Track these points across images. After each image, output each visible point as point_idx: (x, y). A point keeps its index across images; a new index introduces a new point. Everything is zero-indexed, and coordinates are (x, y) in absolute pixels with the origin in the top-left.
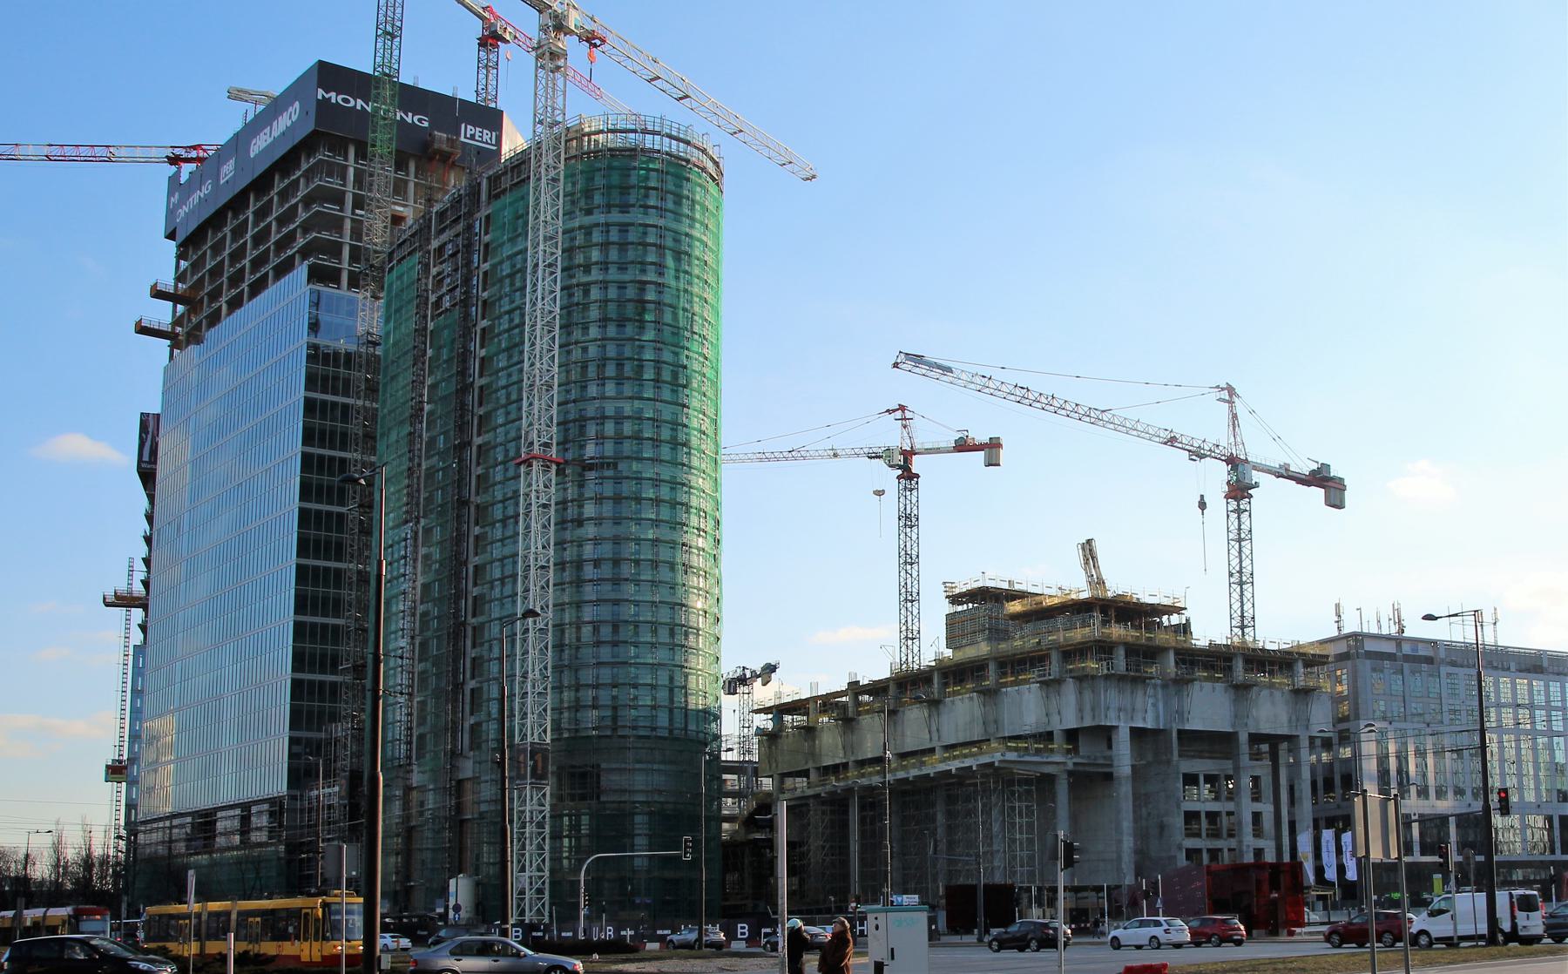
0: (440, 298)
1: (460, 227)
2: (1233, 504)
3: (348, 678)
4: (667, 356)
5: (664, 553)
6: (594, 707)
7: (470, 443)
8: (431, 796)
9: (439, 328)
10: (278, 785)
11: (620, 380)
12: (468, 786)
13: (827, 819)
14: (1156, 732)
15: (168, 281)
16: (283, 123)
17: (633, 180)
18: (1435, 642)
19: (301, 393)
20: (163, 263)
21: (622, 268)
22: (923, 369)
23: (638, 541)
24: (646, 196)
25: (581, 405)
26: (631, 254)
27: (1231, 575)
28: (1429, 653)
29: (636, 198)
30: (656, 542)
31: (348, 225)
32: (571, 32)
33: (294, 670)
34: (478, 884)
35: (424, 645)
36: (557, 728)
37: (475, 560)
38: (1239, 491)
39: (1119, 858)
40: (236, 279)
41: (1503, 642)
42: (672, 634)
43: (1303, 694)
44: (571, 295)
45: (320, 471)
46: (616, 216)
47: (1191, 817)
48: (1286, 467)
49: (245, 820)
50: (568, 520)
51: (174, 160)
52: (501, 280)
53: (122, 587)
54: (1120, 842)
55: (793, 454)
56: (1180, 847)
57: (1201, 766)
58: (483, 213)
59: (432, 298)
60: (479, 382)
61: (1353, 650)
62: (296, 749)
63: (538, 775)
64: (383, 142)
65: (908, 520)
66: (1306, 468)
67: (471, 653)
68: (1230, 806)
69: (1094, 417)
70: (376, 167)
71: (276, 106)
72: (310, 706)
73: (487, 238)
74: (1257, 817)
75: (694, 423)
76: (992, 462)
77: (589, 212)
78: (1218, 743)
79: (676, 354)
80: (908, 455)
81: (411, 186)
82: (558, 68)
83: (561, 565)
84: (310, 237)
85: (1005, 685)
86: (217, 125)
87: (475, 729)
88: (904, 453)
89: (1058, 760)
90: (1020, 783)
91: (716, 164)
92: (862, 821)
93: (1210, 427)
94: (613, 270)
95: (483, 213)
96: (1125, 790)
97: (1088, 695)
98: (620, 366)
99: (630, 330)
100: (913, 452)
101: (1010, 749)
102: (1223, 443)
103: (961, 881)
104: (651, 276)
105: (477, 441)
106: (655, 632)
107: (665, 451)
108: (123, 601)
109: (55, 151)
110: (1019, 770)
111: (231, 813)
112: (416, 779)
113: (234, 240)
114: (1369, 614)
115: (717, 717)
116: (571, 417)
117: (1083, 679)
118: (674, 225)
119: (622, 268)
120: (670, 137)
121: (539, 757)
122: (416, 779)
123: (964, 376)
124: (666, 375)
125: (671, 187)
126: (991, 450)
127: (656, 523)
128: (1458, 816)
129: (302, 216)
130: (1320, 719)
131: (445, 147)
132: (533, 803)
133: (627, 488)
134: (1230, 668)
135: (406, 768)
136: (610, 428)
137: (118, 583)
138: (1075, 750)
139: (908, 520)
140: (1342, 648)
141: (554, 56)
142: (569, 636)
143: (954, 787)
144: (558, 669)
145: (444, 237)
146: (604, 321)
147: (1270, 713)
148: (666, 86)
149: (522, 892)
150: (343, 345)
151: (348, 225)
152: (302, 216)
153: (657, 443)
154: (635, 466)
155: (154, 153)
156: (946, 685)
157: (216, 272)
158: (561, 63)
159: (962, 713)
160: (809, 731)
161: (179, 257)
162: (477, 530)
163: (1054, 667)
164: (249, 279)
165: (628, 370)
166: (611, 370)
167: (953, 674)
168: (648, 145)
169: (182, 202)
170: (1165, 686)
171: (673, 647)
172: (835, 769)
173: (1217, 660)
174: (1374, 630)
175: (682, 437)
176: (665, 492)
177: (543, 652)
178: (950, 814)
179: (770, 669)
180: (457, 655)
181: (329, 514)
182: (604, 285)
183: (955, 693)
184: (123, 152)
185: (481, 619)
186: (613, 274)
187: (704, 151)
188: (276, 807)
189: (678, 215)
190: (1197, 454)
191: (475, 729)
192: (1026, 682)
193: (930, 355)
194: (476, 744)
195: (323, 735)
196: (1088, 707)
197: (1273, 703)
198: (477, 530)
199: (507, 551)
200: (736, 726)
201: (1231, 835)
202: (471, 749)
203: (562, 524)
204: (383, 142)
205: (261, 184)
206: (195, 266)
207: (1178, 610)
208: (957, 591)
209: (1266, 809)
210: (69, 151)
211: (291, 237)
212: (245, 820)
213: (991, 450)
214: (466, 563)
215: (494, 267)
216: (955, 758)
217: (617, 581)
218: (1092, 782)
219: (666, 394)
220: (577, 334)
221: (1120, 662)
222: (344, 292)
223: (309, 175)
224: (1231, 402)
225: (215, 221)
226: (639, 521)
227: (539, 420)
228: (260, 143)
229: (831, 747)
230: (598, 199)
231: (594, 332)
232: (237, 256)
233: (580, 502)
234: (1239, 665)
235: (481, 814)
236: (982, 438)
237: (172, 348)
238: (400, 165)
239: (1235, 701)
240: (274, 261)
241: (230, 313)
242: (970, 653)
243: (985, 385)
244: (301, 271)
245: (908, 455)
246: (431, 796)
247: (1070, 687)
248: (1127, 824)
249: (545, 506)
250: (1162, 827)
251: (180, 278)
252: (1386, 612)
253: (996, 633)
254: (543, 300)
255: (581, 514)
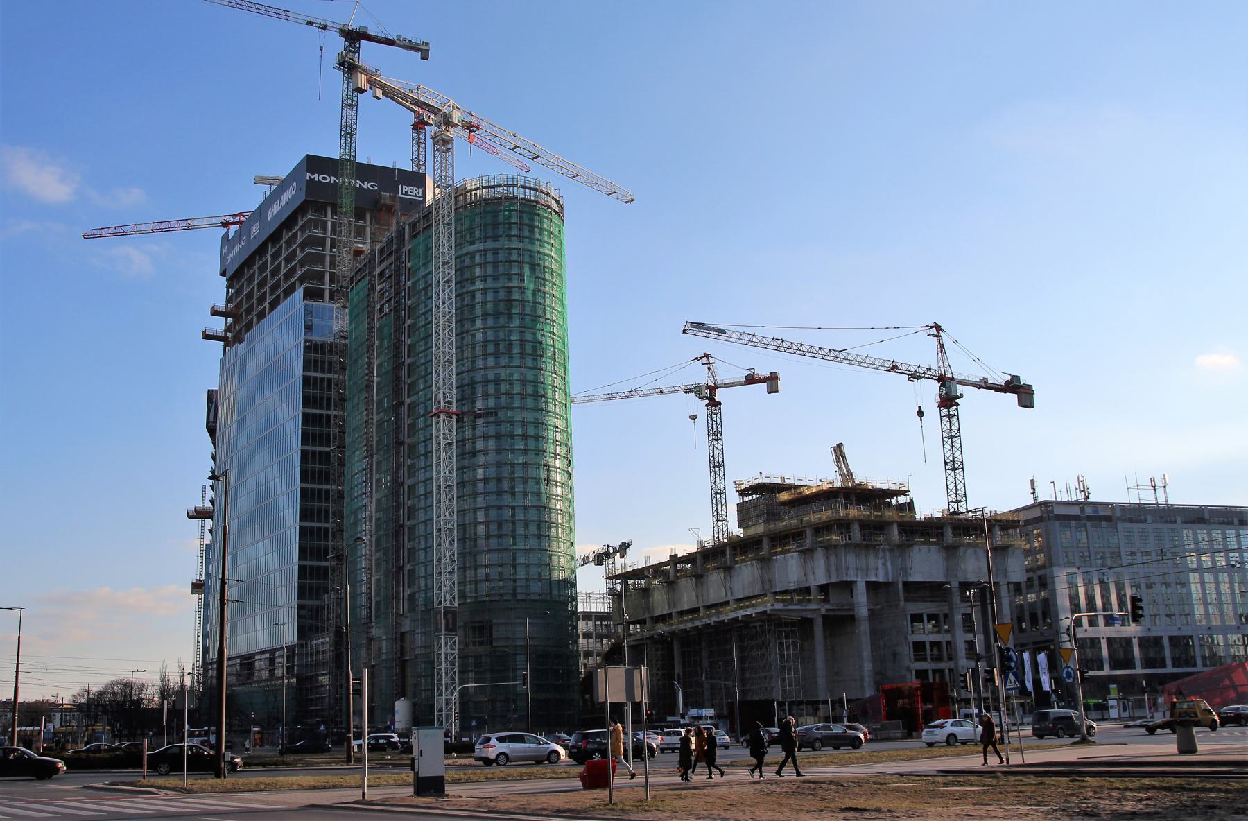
0: (382, 306)
1: (393, 258)
2: (945, 412)
3: (334, 563)
4: (529, 337)
5: (532, 472)
6: (487, 580)
7: (403, 403)
8: (384, 644)
9: (390, 321)
10: (292, 638)
11: (497, 355)
12: (408, 636)
13: (659, 653)
14: (886, 585)
15: (221, 303)
16: (287, 196)
17: (501, 219)
18: (1111, 504)
19: (300, 373)
20: (218, 292)
21: (496, 279)
22: (705, 333)
23: (513, 465)
24: (510, 229)
25: (472, 374)
26: (501, 269)
27: (946, 463)
28: (1109, 513)
29: (508, 227)
30: (525, 465)
31: (328, 259)
32: (456, 125)
33: (300, 559)
34: (414, 705)
35: (378, 541)
36: (462, 595)
37: (408, 482)
38: (948, 401)
39: (862, 679)
40: (262, 300)
41: (1172, 501)
42: (539, 528)
43: (1000, 550)
44: (463, 300)
45: (314, 424)
46: (490, 244)
47: (919, 647)
48: (985, 381)
49: (272, 661)
50: (466, 453)
51: (226, 224)
52: (419, 292)
53: (199, 505)
54: (861, 667)
55: (633, 394)
56: (909, 669)
57: (924, 608)
58: (407, 247)
59: (378, 307)
60: (408, 361)
61: (1045, 516)
62: (303, 612)
63: (451, 629)
64: (347, 203)
65: (715, 436)
66: (1002, 380)
67: (407, 545)
68: (948, 637)
69: (834, 356)
70: (344, 220)
71: (283, 185)
72: (313, 581)
73: (409, 265)
74: (971, 645)
75: (550, 381)
76: (773, 390)
77: (472, 243)
78: (934, 590)
79: (534, 334)
80: (712, 389)
81: (368, 229)
82: (448, 150)
83: (461, 484)
84: (304, 269)
85: (776, 554)
86: (250, 200)
87: (412, 597)
88: (709, 387)
89: (816, 607)
90: (787, 625)
91: (557, 202)
92: (683, 655)
93: (924, 355)
94: (489, 280)
95: (407, 247)
96: (864, 628)
97: (833, 558)
98: (497, 345)
99: (502, 320)
100: (716, 387)
101: (777, 601)
102: (934, 366)
103: (749, 698)
104: (515, 283)
105: (408, 401)
106: (526, 526)
107: (530, 403)
108: (200, 514)
109: (157, 226)
110: (783, 616)
111: (263, 656)
112: (375, 632)
113: (260, 274)
114: (1057, 487)
115: (574, 585)
116: (466, 382)
117: (829, 548)
118: (529, 247)
119: (496, 279)
120: (525, 187)
121: (449, 616)
122: (375, 632)
123: (734, 335)
124: (529, 350)
125: (526, 221)
126: (772, 381)
127: (525, 452)
128: (1140, 639)
129: (300, 256)
130: (1016, 569)
131: (388, 202)
132: (447, 649)
133: (505, 429)
134: (942, 534)
135: (368, 624)
136: (491, 389)
137: (196, 502)
138: (826, 601)
139: (715, 436)
140: (1036, 513)
141: (445, 142)
142: (470, 531)
143: (741, 628)
144: (462, 555)
145: (384, 265)
146: (485, 315)
147: (973, 567)
148: (524, 152)
149: (441, 710)
150: (329, 339)
151: (328, 259)
152: (300, 256)
153: (523, 396)
154: (509, 413)
155: (214, 221)
156: (735, 555)
157: (250, 295)
158: (450, 146)
159: (747, 575)
160: (646, 592)
161: (229, 287)
162: (409, 462)
163: (809, 539)
164: (269, 299)
165: (500, 348)
166: (491, 349)
167: (739, 547)
168: (516, 194)
169: (229, 252)
170: (891, 550)
171: (540, 537)
172: (664, 618)
173: (932, 528)
174: (1065, 499)
175: (541, 391)
176: (531, 430)
177: (451, 544)
178: (741, 649)
179: (625, 546)
180: (398, 548)
181: (321, 453)
182: (485, 291)
183: (743, 561)
184: (196, 223)
185: (413, 522)
186: (490, 283)
187: (548, 194)
188: (291, 652)
189: (532, 240)
190: (914, 377)
191: (412, 597)
192: (789, 551)
193: (709, 322)
194: (412, 608)
195: (319, 603)
196: (833, 568)
197: (977, 559)
198: (409, 462)
199: (428, 475)
200: (592, 590)
201: (950, 659)
202: (409, 611)
203: (461, 455)
204: (347, 203)
205: (275, 237)
206: (238, 293)
207: (904, 493)
208: (743, 487)
209: (979, 639)
210: (164, 225)
211: (293, 270)
212: (272, 661)
213: (772, 381)
214: (402, 484)
215: (414, 283)
216: (741, 608)
217: (500, 493)
218: (839, 623)
219: (529, 362)
220: (468, 326)
221: (857, 535)
222: (327, 304)
223: (303, 229)
224: (938, 336)
225: (249, 262)
226: (513, 451)
227: (443, 385)
228: (274, 210)
229: (660, 602)
230: (478, 234)
231: (479, 324)
232: (262, 284)
233: (474, 440)
234: (949, 532)
235: (416, 656)
236: (765, 373)
237: (225, 346)
238: (359, 215)
239: (947, 559)
240: (284, 286)
241: (258, 321)
242: (753, 531)
243: (750, 340)
244: (300, 292)
245: (712, 389)
246: (384, 644)
247: (820, 555)
248: (866, 653)
249: (450, 444)
250: (895, 655)
251: (229, 301)
252: (1074, 484)
253: (772, 514)
254: (444, 303)
255: (474, 447)
